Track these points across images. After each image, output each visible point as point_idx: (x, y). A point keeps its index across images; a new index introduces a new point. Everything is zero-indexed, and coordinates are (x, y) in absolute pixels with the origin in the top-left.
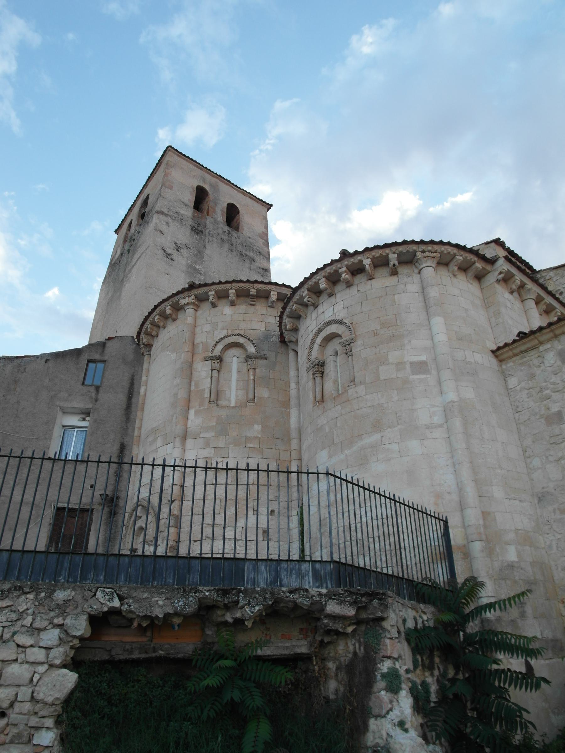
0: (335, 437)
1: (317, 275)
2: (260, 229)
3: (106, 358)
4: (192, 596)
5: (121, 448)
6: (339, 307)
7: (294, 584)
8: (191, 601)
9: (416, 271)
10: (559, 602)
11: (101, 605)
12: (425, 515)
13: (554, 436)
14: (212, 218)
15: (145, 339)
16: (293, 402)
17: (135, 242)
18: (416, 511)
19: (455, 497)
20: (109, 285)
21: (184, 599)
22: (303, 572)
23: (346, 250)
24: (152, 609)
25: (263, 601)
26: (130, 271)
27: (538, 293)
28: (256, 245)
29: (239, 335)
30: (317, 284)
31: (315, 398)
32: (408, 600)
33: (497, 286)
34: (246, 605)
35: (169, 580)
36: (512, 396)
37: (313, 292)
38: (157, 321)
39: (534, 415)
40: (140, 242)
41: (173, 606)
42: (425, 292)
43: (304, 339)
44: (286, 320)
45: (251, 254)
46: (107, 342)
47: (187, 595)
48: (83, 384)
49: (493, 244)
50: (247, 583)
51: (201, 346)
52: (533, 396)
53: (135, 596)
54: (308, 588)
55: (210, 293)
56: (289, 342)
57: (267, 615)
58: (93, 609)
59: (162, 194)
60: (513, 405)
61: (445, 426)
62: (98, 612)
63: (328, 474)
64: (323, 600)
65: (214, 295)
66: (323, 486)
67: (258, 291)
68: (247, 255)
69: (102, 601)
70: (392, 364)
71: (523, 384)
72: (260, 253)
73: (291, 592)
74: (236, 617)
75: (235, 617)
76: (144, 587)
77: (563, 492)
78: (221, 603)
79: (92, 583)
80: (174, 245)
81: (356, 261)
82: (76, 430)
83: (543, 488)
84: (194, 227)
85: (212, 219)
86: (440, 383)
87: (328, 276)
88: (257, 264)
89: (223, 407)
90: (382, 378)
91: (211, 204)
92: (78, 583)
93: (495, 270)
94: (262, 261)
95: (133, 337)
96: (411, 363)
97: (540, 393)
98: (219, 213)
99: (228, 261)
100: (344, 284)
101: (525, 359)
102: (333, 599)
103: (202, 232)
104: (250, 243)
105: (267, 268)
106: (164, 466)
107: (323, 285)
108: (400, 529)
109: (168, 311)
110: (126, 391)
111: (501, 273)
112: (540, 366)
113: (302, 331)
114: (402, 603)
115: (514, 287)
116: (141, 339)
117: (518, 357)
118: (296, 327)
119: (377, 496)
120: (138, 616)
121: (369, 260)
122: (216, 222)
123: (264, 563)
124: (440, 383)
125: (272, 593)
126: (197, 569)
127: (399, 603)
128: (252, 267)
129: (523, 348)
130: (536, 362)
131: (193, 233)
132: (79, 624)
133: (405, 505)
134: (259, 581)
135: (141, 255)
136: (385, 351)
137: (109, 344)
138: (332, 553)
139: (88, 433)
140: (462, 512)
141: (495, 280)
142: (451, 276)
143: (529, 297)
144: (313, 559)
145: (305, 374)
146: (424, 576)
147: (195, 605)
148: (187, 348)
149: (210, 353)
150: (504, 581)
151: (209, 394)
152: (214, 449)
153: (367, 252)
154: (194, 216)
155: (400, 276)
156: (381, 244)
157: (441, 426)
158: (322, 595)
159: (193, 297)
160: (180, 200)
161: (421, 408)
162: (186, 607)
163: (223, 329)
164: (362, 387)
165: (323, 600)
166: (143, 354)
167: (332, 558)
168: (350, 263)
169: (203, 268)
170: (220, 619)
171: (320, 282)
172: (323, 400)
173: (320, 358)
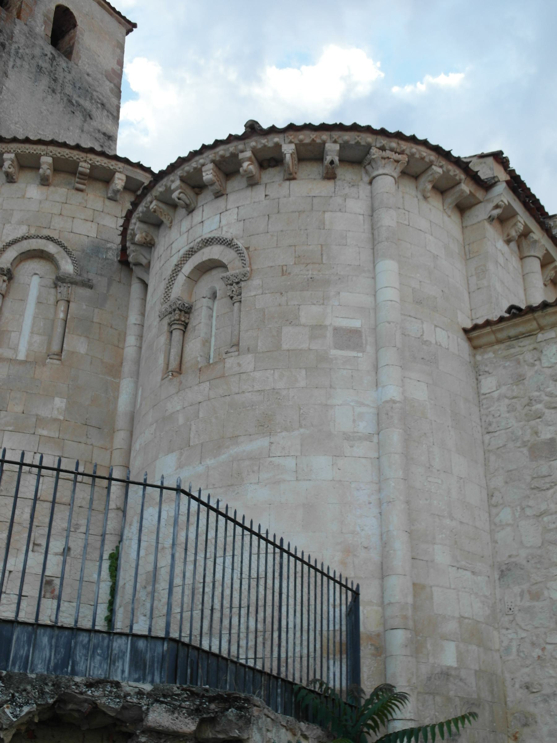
0: (192, 435)
1: (201, 156)
2: (110, 64)
6: (230, 217)
7: (96, 672)
9: (366, 179)
10: (509, 737)
12: (325, 579)
13: (538, 477)
14: (26, 24)
16: (127, 367)
18: (312, 571)
19: (374, 555)
22: (115, 652)
23: (257, 123)
25: (39, 698)
27: (547, 250)
28: (98, 89)
29: (48, 238)
30: (198, 171)
31: (168, 365)
32: (281, 713)
33: (487, 225)
34: (6, 702)
36: (484, 407)
37: (189, 185)
39: (514, 441)
42: (375, 215)
43: (162, 262)
44: (135, 225)
45: (87, 104)
49: (491, 160)
50: (14, 664)
52: (515, 410)
54: (120, 681)
55: (6, 156)
60: (483, 420)
61: (375, 439)
64: (144, 702)
65: (12, 161)
66: (168, 510)
67: (93, 167)
68: (79, 105)
70: (304, 326)
71: (504, 389)
72: (103, 104)
73: (89, 685)
77: (539, 566)
81: (270, 144)
83: (510, 556)
85: (25, 27)
86: (376, 368)
88: (94, 123)
90: (285, 347)
93: (488, 201)
94: (104, 121)
96: (335, 329)
97: (527, 408)
98: (40, 19)
99: (44, 107)
100: (245, 179)
101: (512, 351)
102: (162, 702)
105: (111, 134)
107: (208, 175)
108: (284, 596)
111: (497, 207)
112: (533, 365)
114: (273, 717)
115: (513, 233)
117: (502, 346)
118: (151, 240)
119: (255, 538)
121: (293, 146)
122: (31, 34)
123: (49, 630)
124: (376, 368)
127: (268, 717)
128: (86, 127)
129: (513, 332)
130: (529, 357)
133: (296, 558)
134: (36, 662)
136: (296, 303)
138: (168, 625)
140: (383, 581)
141: (487, 217)
142: (420, 197)
143: (532, 253)
144: (134, 632)
146: (311, 677)
150: (431, 697)
153: (291, 133)
155: (338, 183)
156: (316, 123)
157: (368, 438)
158: (144, 694)
161: (341, 405)
165: (144, 702)
167: (168, 632)
168: (259, 146)
171: (204, 169)
172: (179, 371)
173: (186, 299)
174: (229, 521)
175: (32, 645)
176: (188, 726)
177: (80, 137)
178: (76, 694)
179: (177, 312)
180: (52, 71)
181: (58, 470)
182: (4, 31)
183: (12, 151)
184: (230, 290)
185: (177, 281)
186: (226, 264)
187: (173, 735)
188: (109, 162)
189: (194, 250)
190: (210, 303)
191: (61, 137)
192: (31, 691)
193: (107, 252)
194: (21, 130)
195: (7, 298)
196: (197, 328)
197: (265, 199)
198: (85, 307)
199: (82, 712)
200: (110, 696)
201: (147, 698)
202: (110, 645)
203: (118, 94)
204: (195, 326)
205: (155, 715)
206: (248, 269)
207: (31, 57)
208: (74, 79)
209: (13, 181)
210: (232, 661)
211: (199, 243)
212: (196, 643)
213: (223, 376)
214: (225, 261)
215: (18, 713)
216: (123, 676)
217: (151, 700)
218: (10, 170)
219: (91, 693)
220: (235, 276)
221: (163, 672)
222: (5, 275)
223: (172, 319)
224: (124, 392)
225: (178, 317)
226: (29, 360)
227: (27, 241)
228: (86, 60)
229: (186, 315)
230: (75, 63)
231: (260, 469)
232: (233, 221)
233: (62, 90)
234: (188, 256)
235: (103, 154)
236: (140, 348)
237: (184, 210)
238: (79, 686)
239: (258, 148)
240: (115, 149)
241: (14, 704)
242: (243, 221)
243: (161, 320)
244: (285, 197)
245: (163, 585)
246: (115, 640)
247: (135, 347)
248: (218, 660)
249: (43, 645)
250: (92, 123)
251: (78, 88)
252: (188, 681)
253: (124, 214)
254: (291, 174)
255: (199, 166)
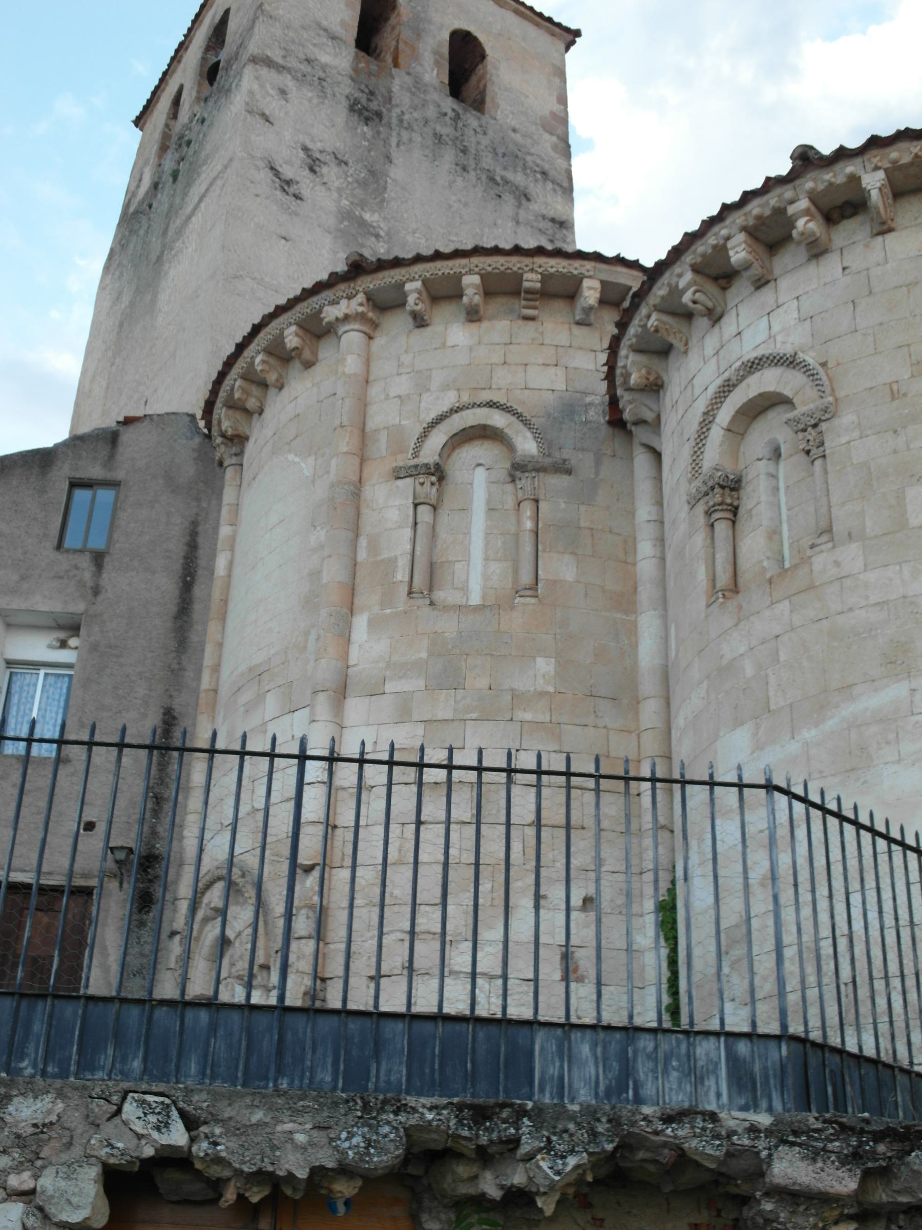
0: (771, 693)
1: (722, 225)
2: (547, 105)
3: (120, 475)
4: (388, 1123)
5: (165, 722)
6: (787, 316)
7: (674, 1098)
8: (385, 1136)
11: (135, 1141)
14: (408, 74)
15: (225, 420)
16: (646, 594)
17: (191, 151)
20: (121, 274)
21: (366, 1129)
22: (700, 1063)
24: (278, 1153)
25: (589, 1142)
26: (180, 232)
28: (533, 150)
29: (491, 405)
30: (721, 250)
31: (713, 580)
34: (540, 1150)
35: (321, 1076)
37: (708, 276)
38: (259, 368)
40: (208, 148)
41: (336, 1148)
43: (681, 412)
44: (627, 359)
45: (518, 178)
46: (121, 429)
47: (374, 1118)
48: (59, 546)
50: (542, 1090)
51: (383, 437)
53: (230, 1118)
54: (717, 1111)
55: (408, 287)
56: (636, 423)
57: (597, 1181)
58: (115, 1152)
59: (266, 7)
62: (128, 1158)
63: (770, 787)
64: (761, 1144)
65: (420, 293)
66: (757, 820)
67: (546, 278)
68: (506, 182)
69: (140, 1130)
72: (544, 173)
73: (668, 1119)
74: (512, 1186)
75: (508, 1183)
76: (253, 1094)
78: (469, 1144)
79: (110, 1079)
80: (302, 154)
81: (840, 179)
82: (42, 672)
84: (356, 102)
85: (408, 80)
87: (756, 227)
88: (534, 207)
89: (447, 608)
91: (406, 34)
92: (72, 1079)
95: (193, 417)
98: (428, 59)
99: (454, 198)
102: (793, 1144)
103: (379, 115)
104: (516, 144)
105: (564, 218)
106: (302, 758)
107: (738, 253)
109: (292, 339)
110: (177, 566)
113: (674, 391)
116: (215, 422)
118: (656, 379)
120: (239, 1173)
121: (881, 174)
122: (418, 86)
123: (589, 1033)
125: (614, 1121)
126: (399, 1046)
128: (523, 215)
131: (356, 117)
132: (77, 1190)
134: (576, 1084)
135: (211, 184)
137: (128, 436)
139: (75, 680)
144: (728, 1028)
145: (683, 515)
147: (397, 1148)
148: (346, 443)
149: (410, 456)
151: (407, 572)
152: (422, 725)
153: (875, 152)
154: (356, 70)
158: (759, 1131)
159: (361, 297)
160: (319, 25)
162: (372, 1151)
163: (445, 387)
164: (854, 548)
166: (221, 464)
167: (784, 1026)
168: (821, 187)
169: (385, 218)
170: (464, 1189)
171: (730, 244)
172: (735, 588)
173: (729, 467)
174: (862, 832)
175: (566, 1059)
176: (844, 1182)
177: (515, 232)
178: (648, 1135)
179: (717, 490)
180: (457, 138)
181: (568, 774)
182: (377, 92)
183: (417, 277)
184: (803, 439)
185: (709, 439)
186: (791, 397)
187: (819, 1199)
188: (569, 265)
189: (731, 383)
190: (770, 467)
191: (485, 239)
192: (576, 1132)
193: (586, 412)
194: (423, 241)
195: (440, 511)
196: (754, 512)
197: (843, 276)
198: (563, 506)
199: (661, 1163)
200: (703, 1135)
201: (766, 1137)
202: (692, 1051)
203: (565, 151)
204: (751, 510)
205: (784, 1165)
206: (831, 399)
207: (423, 122)
208: (493, 143)
209: (424, 323)
210: (902, 1070)
211: (739, 370)
212: (834, 1040)
213: (811, 587)
214: (788, 392)
215: (560, 1167)
216: (720, 1103)
217: (774, 1141)
218: (418, 308)
219: (673, 1131)
220: (808, 415)
221: (785, 1093)
222: (433, 475)
223: (711, 503)
224: (646, 635)
225: (720, 499)
226: (488, 603)
227: (459, 414)
228: (508, 108)
229: (733, 493)
230: (492, 117)
231: (900, 736)
232: (792, 323)
233: (477, 164)
234: (722, 394)
235: (558, 253)
236: (663, 559)
237: (705, 320)
238: (650, 1121)
239: (819, 190)
240: (574, 242)
241: (552, 1153)
242: (809, 320)
243: (691, 509)
244: (879, 265)
245: (763, 945)
246: (697, 1042)
247: (653, 559)
248: (877, 1068)
249: (584, 1057)
250: (531, 207)
251: (501, 155)
252: (831, 1106)
253: (606, 344)
254: (884, 223)
255: (722, 242)
